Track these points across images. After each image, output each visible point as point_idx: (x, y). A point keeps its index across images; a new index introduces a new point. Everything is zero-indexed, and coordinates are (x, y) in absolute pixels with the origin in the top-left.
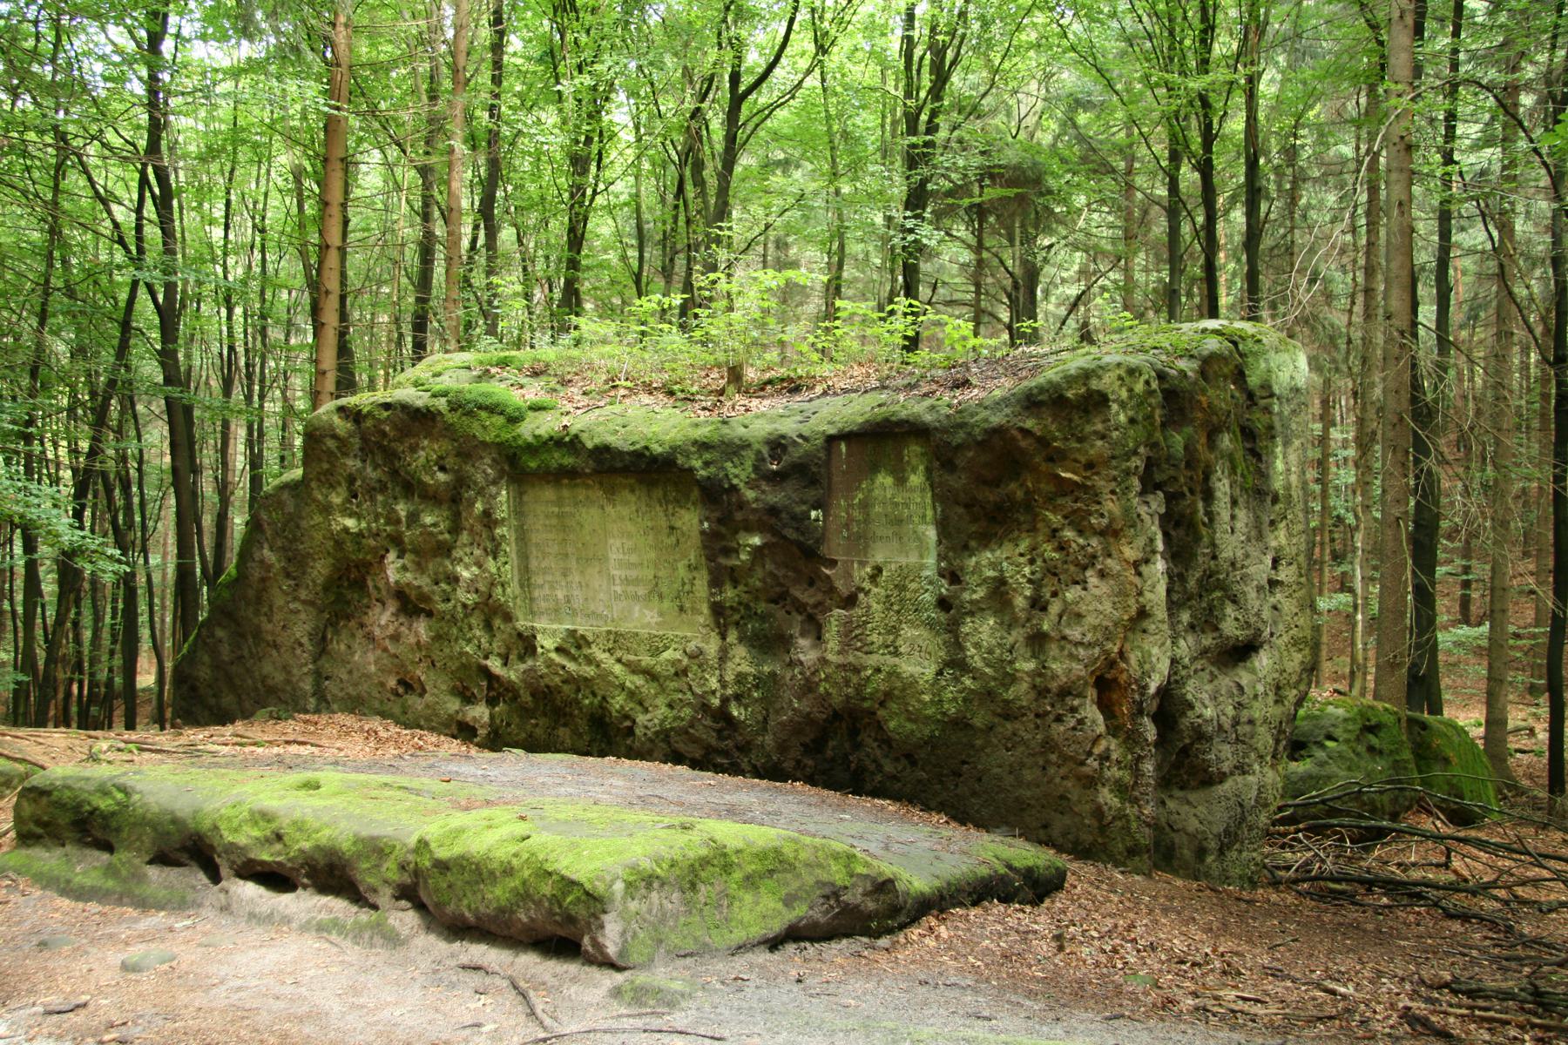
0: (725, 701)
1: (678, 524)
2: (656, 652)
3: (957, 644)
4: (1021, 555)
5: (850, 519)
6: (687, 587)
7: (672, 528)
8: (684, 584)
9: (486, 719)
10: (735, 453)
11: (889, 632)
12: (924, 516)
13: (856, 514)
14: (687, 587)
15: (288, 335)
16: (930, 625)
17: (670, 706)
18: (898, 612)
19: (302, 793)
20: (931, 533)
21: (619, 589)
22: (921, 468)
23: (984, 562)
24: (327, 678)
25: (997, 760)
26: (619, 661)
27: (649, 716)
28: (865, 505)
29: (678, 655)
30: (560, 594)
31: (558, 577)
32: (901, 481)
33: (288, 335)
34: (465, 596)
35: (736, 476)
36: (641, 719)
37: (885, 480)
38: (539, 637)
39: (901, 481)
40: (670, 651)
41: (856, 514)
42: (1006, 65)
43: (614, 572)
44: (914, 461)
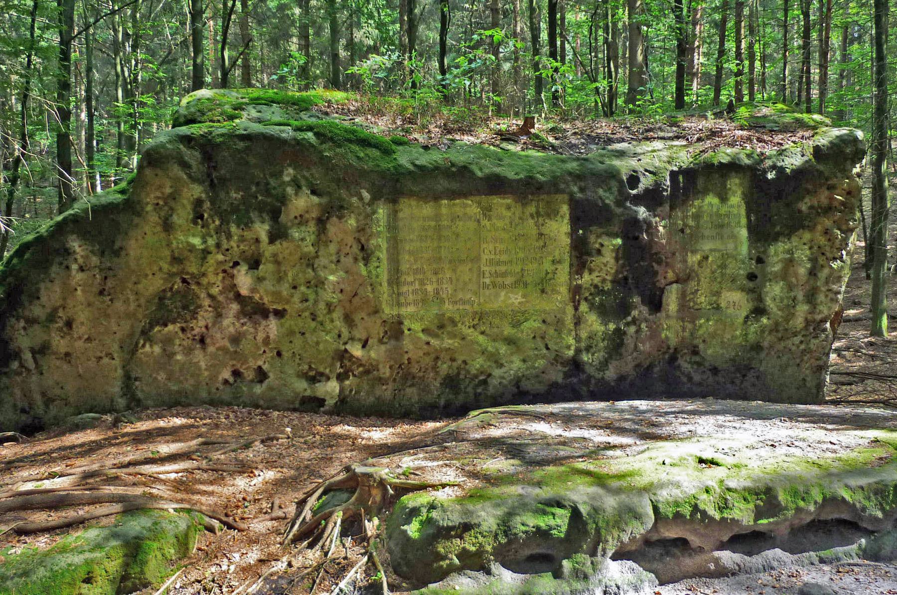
0: (578, 351)
1: (545, 230)
2: (516, 325)
3: (760, 299)
4: (805, 244)
5: (685, 225)
6: (550, 276)
7: (541, 234)
8: (547, 273)
9: (337, 390)
10: (603, 182)
11: (714, 295)
12: (739, 222)
13: (691, 222)
14: (550, 276)
15: (29, 62)
16: (742, 289)
17: (524, 361)
18: (720, 283)
19: (719, 461)
20: (744, 233)
21: (487, 281)
22: (739, 192)
23: (777, 251)
24: (136, 379)
25: (768, 364)
26: (483, 333)
27: (504, 370)
28: (697, 217)
29: (537, 325)
30: (430, 288)
31: (429, 274)
32: (724, 199)
33: (29, 62)
34: (329, 295)
35: (608, 198)
36: (497, 372)
37: (712, 200)
38: (407, 323)
39: (724, 199)
40: (531, 321)
41: (691, 222)
42: (23, 59)
43: (484, 268)
44: (734, 188)
